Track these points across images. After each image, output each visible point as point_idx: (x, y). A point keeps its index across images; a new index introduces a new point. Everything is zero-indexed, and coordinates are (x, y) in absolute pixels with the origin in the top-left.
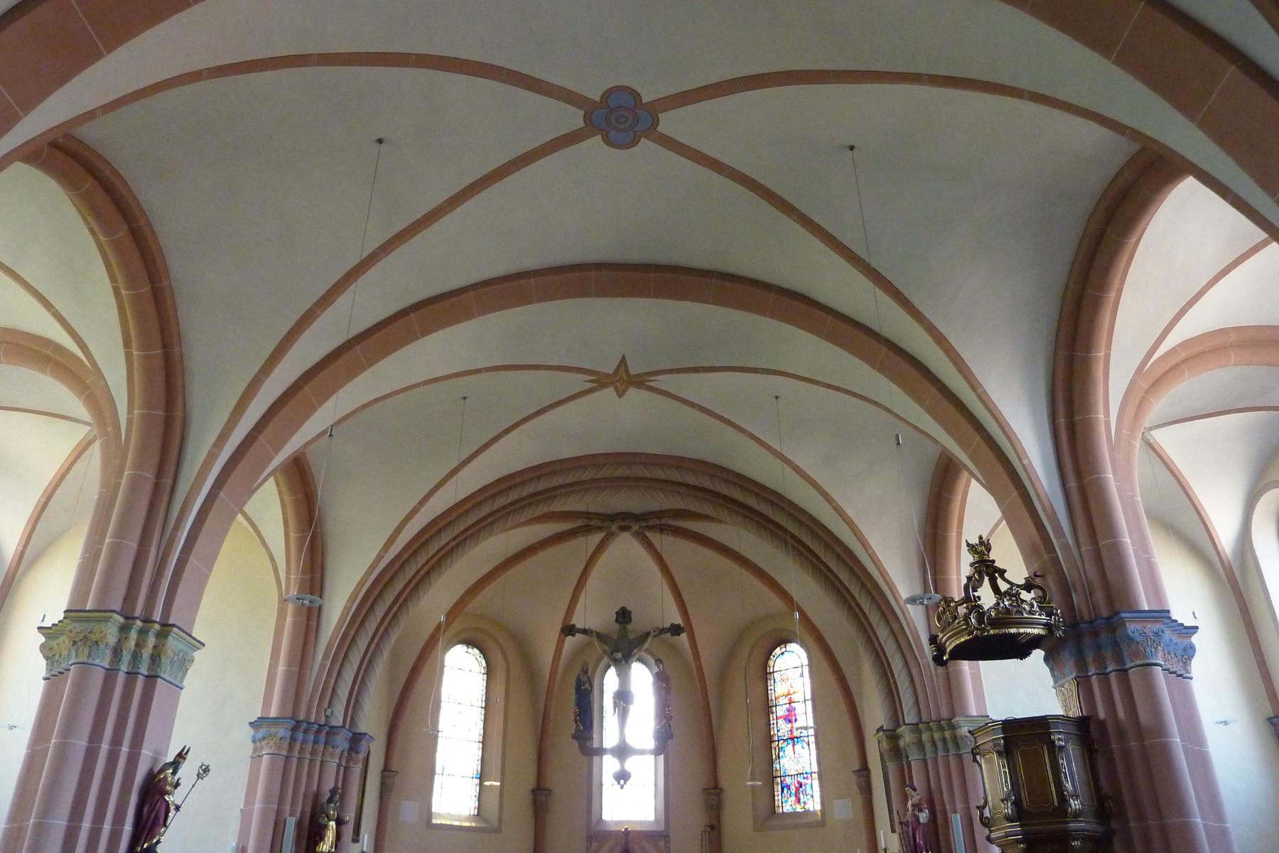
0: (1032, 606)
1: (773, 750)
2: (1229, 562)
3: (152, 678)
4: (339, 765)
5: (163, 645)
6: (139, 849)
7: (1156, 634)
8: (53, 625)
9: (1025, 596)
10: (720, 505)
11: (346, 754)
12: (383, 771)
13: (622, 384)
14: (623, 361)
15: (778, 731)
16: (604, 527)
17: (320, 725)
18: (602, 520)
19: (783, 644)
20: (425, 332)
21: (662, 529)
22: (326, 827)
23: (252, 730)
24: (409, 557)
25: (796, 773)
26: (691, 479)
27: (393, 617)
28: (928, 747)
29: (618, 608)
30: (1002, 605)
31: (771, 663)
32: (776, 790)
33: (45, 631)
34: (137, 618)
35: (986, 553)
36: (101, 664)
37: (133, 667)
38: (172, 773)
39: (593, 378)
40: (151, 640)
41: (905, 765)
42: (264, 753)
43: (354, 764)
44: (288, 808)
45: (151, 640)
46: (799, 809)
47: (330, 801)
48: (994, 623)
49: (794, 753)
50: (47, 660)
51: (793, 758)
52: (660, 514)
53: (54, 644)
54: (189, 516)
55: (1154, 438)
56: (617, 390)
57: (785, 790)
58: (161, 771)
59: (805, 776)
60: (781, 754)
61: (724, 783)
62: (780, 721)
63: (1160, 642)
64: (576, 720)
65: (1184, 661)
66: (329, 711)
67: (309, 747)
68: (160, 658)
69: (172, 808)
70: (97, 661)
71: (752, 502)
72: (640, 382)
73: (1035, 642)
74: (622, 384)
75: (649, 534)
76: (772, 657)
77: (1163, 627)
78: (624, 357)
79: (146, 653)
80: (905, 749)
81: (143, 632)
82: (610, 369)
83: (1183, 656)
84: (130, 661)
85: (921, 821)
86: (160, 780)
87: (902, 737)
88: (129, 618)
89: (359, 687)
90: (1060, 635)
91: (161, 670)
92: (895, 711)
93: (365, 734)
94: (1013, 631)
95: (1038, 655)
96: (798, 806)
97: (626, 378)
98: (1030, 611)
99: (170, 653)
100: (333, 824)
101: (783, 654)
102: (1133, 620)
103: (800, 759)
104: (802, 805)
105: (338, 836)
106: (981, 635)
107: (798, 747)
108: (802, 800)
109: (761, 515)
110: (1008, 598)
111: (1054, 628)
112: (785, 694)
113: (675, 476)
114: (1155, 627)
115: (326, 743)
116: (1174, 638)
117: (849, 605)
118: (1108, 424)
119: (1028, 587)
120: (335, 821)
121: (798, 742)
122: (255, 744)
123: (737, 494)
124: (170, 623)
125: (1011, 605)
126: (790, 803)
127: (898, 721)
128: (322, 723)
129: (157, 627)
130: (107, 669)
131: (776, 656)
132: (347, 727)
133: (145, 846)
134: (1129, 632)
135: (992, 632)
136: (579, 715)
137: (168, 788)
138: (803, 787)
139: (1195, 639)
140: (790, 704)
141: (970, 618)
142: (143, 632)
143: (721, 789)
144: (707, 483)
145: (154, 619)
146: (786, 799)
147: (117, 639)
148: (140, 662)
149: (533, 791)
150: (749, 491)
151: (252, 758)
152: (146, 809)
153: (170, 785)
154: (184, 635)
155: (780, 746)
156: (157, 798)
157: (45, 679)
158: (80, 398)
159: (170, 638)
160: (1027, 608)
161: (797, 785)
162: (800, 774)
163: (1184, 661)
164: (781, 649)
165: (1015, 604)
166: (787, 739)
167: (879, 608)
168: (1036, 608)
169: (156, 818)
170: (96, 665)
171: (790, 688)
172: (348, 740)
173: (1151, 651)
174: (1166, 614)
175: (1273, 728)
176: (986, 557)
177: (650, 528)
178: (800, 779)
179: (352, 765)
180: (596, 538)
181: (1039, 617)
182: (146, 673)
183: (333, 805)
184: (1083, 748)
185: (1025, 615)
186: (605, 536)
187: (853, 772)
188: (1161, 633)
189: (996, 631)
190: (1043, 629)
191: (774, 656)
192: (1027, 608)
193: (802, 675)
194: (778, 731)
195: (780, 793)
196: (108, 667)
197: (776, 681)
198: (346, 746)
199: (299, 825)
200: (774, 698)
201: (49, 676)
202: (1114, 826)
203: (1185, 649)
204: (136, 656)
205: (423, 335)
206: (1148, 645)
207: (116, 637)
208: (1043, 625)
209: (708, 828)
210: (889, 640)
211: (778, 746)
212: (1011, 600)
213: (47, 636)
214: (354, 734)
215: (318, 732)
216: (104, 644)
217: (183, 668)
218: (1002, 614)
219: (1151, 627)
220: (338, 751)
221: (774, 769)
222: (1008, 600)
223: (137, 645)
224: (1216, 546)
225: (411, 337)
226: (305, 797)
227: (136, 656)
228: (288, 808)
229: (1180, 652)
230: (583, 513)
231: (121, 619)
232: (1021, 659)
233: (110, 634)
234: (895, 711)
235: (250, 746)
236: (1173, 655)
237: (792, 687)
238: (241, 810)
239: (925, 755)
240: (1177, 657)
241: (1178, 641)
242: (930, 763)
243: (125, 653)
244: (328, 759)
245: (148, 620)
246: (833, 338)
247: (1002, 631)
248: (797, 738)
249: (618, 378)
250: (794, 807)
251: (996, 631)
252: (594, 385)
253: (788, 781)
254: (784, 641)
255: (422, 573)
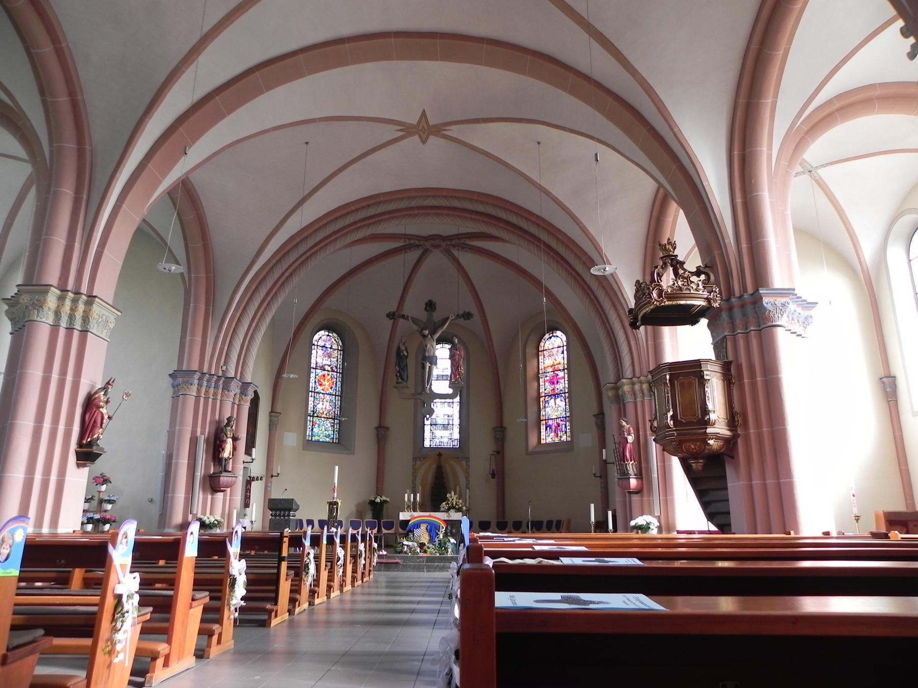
0: (698, 285)
1: (541, 403)
2: (868, 268)
3: (84, 332)
4: (233, 403)
5: (90, 310)
6: (85, 442)
7: (783, 305)
8: (12, 297)
9: (694, 279)
10: (502, 228)
11: (238, 396)
12: (270, 412)
13: (424, 133)
14: (424, 114)
15: (545, 390)
16: (421, 245)
17: (218, 377)
18: (419, 240)
19: (550, 331)
20: (269, 88)
21: (464, 247)
22: (225, 442)
23: (172, 380)
24: (276, 263)
25: (556, 417)
26: (480, 208)
27: (267, 305)
28: (639, 395)
29: (426, 301)
30: (676, 285)
31: (542, 344)
32: (542, 429)
33: (7, 301)
34: (69, 291)
35: (672, 250)
36: (46, 321)
37: (70, 325)
38: (104, 395)
39: (402, 128)
40: (81, 307)
41: (622, 407)
42: (180, 394)
43: (245, 403)
44: (199, 430)
45: (81, 307)
46: (557, 440)
47: (228, 424)
48: (670, 297)
49: (555, 404)
50: (11, 321)
51: (554, 408)
52: (459, 236)
53: (14, 310)
54: (101, 221)
55: (819, 175)
56: (420, 137)
57: (548, 429)
58: (96, 393)
59: (562, 419)
60: (547, 405)
61: (505, 424)
62: (547, 384)
63: (785, 311)
64: (396, 375)
65: (805, 326)
66: (224, 368)
67: (212, 391)
68: (89, 319)
69: (106, 417)
70: (44, 320)
71: (524, 224)
72: (438, 130)
73: (702, 313)
74: (424, 133)
75: (455, 252)
76: (543, 340)
77: (789, 301)
78: (424, 110)
79: (79, 314)
80: (622, 395)
81: (75, 301)
82: (414, 121)
83: (804, 323)
84: (67, 320)
85: (629, 441)
86: (95, 399)
87: (621, 387)
88: (64, 290)
89: (246, 353)
90: (716, 306)
91: (90, 327)
92: (618, 371)
93: (251, 383)
94: (682, 302)
95: (704, 322)
96: (556, 439)
97: (426, 128)
98: (696, 289)
99: (95, 315)
100: (230, 441)
101: (550, 338)
102: (768, 295)
103: (559, 408)
104: (559, 438)
105: (234, 448)
106: (660, 305)
107: (558, 401)
108: (559, 435)
109: (531, 235)
110: (681, 280)
111: (712, 301)
112: (551, 365)
113: (468, 205)
114: (783, 300)
115: (223, 389)
116: (799, 310)
117: (590, 298)
118: (770, 156)
119: (698, 273)
120: (232, 438)
121: (558, 397)
122: (174, 389)
123: (513, 219)
124: (94, 295)
125: (683, 285)
126: (551, 437)
127: (619, 377)
128: (220, 375)
129: (84, 297)
130: (52, 326)
131: (546, 339)
132: (238, 378)
133: (89, 440)
134: (764, 303)
135: (667, 303)
136: (399, 372)
137: (101, 404)
138: (561, 427)
139: (813, 312)
140: (554, 371)
141: (652, 293)
142: (75, 301)
143: (505, 428)
144: (491, 211)
145: (82, 291)
146: (548, 434)
147: (57, 305)
148: (74, 321)
149: (376, 428)
150: (522, 216)
151: (173, 397)
152: (87, 417)
153: (103, 402)
154: (104, 303)
155: (546, 400)
156: (95, 410)
157: (11, 334)
158: (15, 137)
159: (94, 305)
160: (695, 287)
161: (556, 425)
162: (559, 418)
163: (805, 326)
164: (549, 335)
165: (686, 284)
166: (551, 395)
167: (611, 299)
168: (701, 287)
169: (95, 422)
170: (43, 322)
171: (555, 361)
172: (239, 387)
173: (778, 317)
174: (792, 292)
175: (883, 385)
176: (671, 253)
177: (454, 246)
178: (559, 421)
179: (242, 403)
180: (414, 255)
181: (702, 293)
182: (80, 329)
183: (229, 428)
184: (724, 381)
185: (692, 292)
186: (423, 252)
187: (594, 415)
188: (786, 304)
189: (670, 303)
190: (704, 301)
191: (544, 340)
192: (695, 287)
193: (563, 352)
194: (545, 390)
195: (544, 430)
196: (52, 324)
197: (546, 356)
198: (238, 391)
199: (207, 441)
200: (543, 368)
201: (13, 331)
202: (739, 432)
203: (806, 318)
204: (71, 317)
205: (267, 90)
206: (776, 312)
207: (55, 304)
208: (704, 298)
209: (495, 453)
210: (617, 320)
211: (545, 399)
212: (683, 281)
213: (10, 306)
214: (243, 383)
215: (217, 382)
216: (47, 308)
217: (107, 327)
218: (676, 291)
219: (780, 301)
220: (232, 394)
221: (541, 415)
222: (681, 281)
223: (71, 309)
224: (860, 259)
225: (257, 92)
226: (210, 423)
227: (71, 317)
228: (199, 430)
229: (802, 320)
230: (402, 235)
231: (58, 292)
232: (692, 325)
233: (50, 301)
234: (618, 371)
235: (172, 389)
236: (796, 321)
237: (556, 360)
238: (168, 431)
239: (635, 399)
240: (799, 323)
241: (802, 312)
242: (639, 405)
243: (63, 315)
244: (225, 399)
245: (77, 293)
246: (574, 92)
247: (674, 303)
248: (558, 394)
249: (420, 128)
250: (554, 440)
251: (670, 303)
252: (401, 133)
253: (550, 422)
254: (552, 329)
255: (287, 274)
